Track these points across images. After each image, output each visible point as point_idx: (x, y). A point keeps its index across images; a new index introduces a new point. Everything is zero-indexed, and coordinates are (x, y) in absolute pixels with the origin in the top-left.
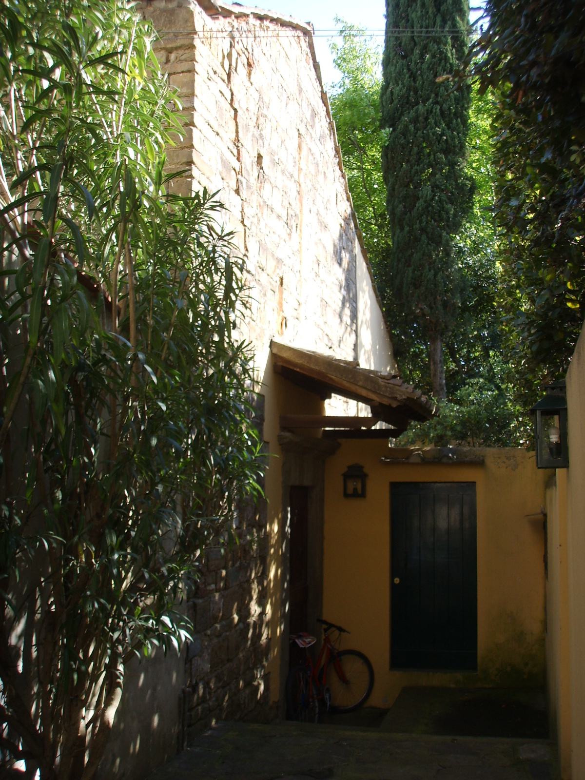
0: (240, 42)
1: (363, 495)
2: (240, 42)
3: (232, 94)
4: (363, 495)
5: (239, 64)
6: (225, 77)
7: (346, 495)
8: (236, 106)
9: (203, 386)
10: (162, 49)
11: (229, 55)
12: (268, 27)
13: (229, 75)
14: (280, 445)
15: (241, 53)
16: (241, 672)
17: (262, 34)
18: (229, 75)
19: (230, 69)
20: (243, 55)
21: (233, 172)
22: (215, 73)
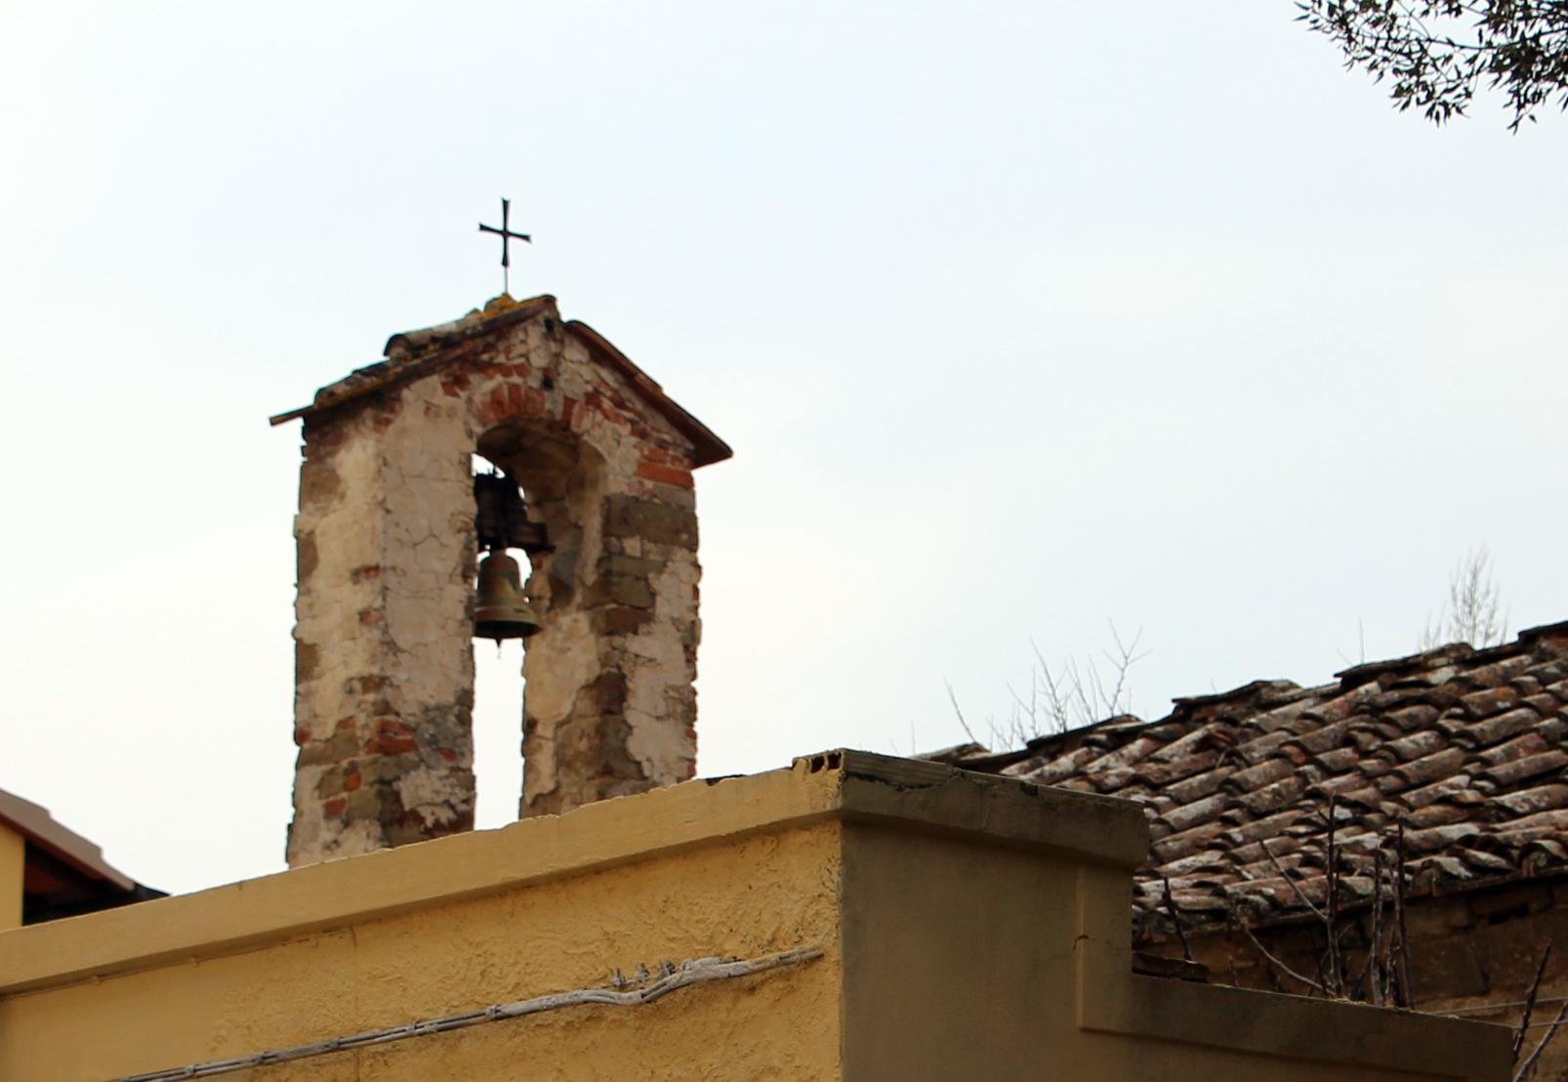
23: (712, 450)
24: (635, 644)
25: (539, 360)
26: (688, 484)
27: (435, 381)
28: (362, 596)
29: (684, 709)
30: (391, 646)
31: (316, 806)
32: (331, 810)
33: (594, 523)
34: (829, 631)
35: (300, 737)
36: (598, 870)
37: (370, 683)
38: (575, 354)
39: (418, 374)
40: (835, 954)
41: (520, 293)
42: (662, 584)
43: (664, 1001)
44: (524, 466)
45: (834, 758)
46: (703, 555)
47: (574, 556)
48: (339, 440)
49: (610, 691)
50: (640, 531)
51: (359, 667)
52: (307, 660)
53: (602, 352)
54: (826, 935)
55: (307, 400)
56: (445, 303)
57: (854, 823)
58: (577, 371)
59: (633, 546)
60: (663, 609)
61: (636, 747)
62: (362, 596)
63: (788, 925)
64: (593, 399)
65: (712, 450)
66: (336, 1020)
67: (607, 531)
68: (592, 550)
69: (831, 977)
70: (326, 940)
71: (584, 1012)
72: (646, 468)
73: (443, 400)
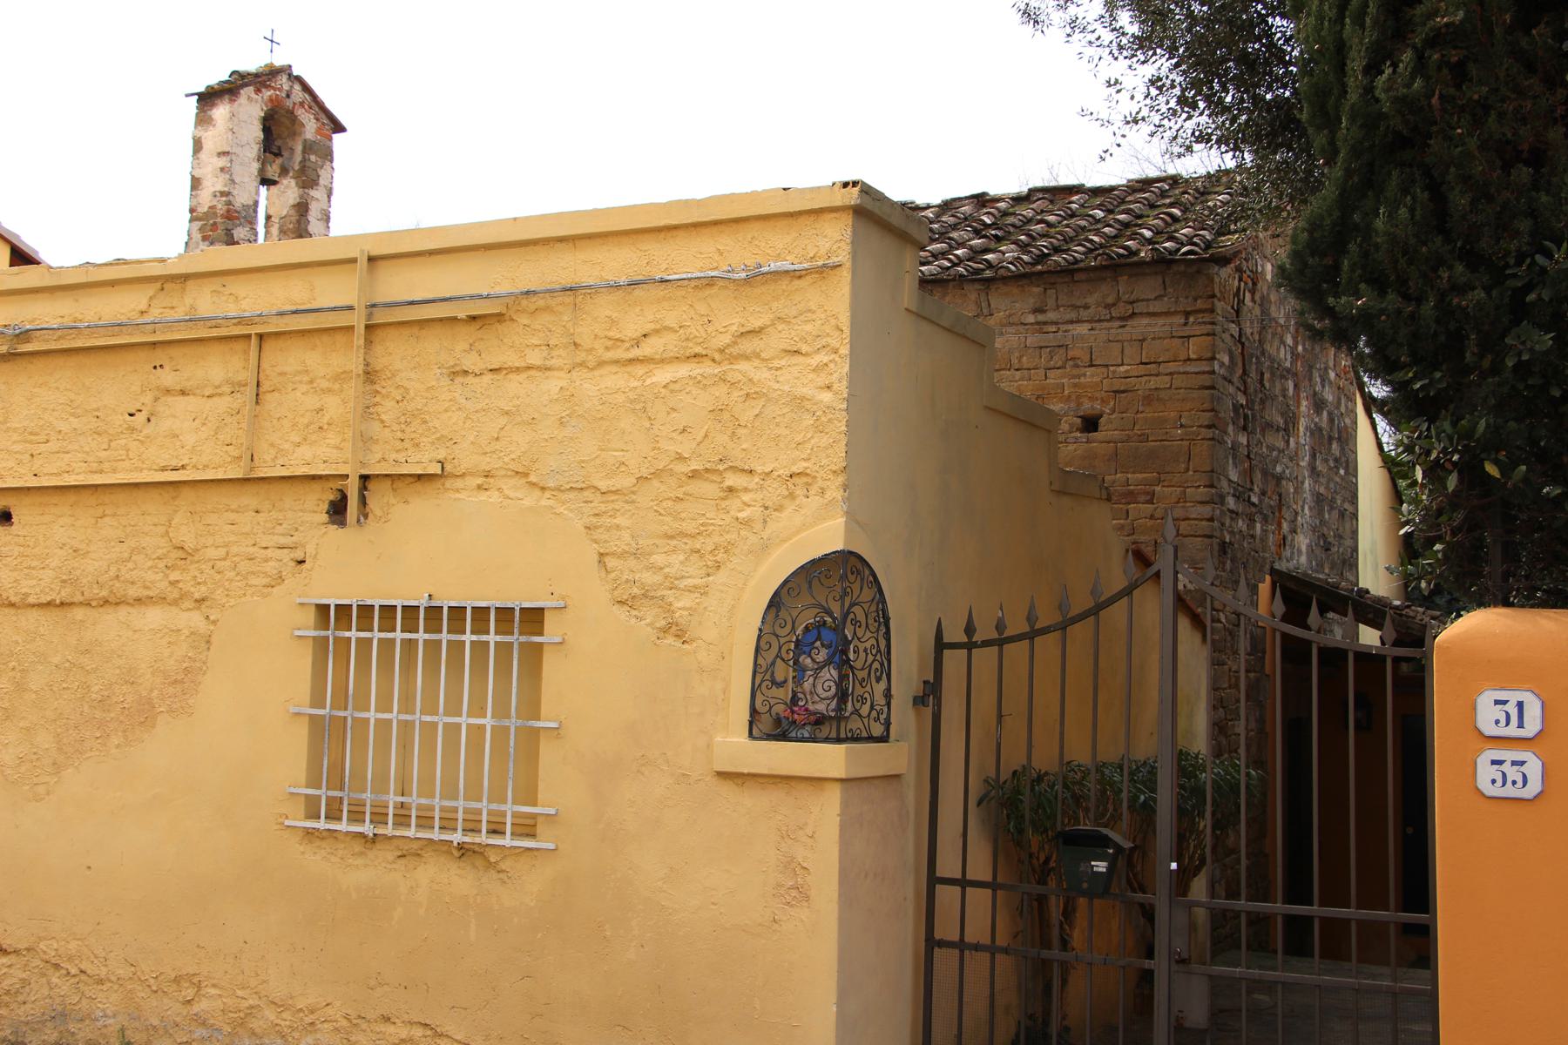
23: (339, 128)
24: (312, 193)
25: (286, 87)
26: (331, 139)
27: (252, 88)
28: (223, 162)
29: (326, 218)
30: (233, 181)
31: (197, 236)
32: (205, 239)
33: (299, 148)
34: (367, 195)
35: (192, 211)
36: (716, 223)
37: (223, 194)
38: (297, 87)
39: (246, 85)
40: (848, 265)
41: (278, 63)
42: (322, 172)
43: (757, 278)
44: (284, 126)
45: (855, 184)
46: (335, 164)
47: (290, 159)
48: (213, 105)
49: (302, 208)
50: (315, 153)
51: (220, 187)
52: (196, 183)
53: (306, 88)
54: (843, 255)
55: (202, 89)
56: (252, 63)
57: (859, 212)
58: (298, 94)
59: (313, 158)
60: (322, 181)
61: (311, 229)
62: (223, 162)
63: (823, 251)
64: (302, 104)
65: (339, 128)
66: (567, 279)
67: (304, 151)
68: (298, 157)
69: (846, 275)
70: (559, 245)
71: (705, 282)
72: (318, 131)
73: (253, 95)
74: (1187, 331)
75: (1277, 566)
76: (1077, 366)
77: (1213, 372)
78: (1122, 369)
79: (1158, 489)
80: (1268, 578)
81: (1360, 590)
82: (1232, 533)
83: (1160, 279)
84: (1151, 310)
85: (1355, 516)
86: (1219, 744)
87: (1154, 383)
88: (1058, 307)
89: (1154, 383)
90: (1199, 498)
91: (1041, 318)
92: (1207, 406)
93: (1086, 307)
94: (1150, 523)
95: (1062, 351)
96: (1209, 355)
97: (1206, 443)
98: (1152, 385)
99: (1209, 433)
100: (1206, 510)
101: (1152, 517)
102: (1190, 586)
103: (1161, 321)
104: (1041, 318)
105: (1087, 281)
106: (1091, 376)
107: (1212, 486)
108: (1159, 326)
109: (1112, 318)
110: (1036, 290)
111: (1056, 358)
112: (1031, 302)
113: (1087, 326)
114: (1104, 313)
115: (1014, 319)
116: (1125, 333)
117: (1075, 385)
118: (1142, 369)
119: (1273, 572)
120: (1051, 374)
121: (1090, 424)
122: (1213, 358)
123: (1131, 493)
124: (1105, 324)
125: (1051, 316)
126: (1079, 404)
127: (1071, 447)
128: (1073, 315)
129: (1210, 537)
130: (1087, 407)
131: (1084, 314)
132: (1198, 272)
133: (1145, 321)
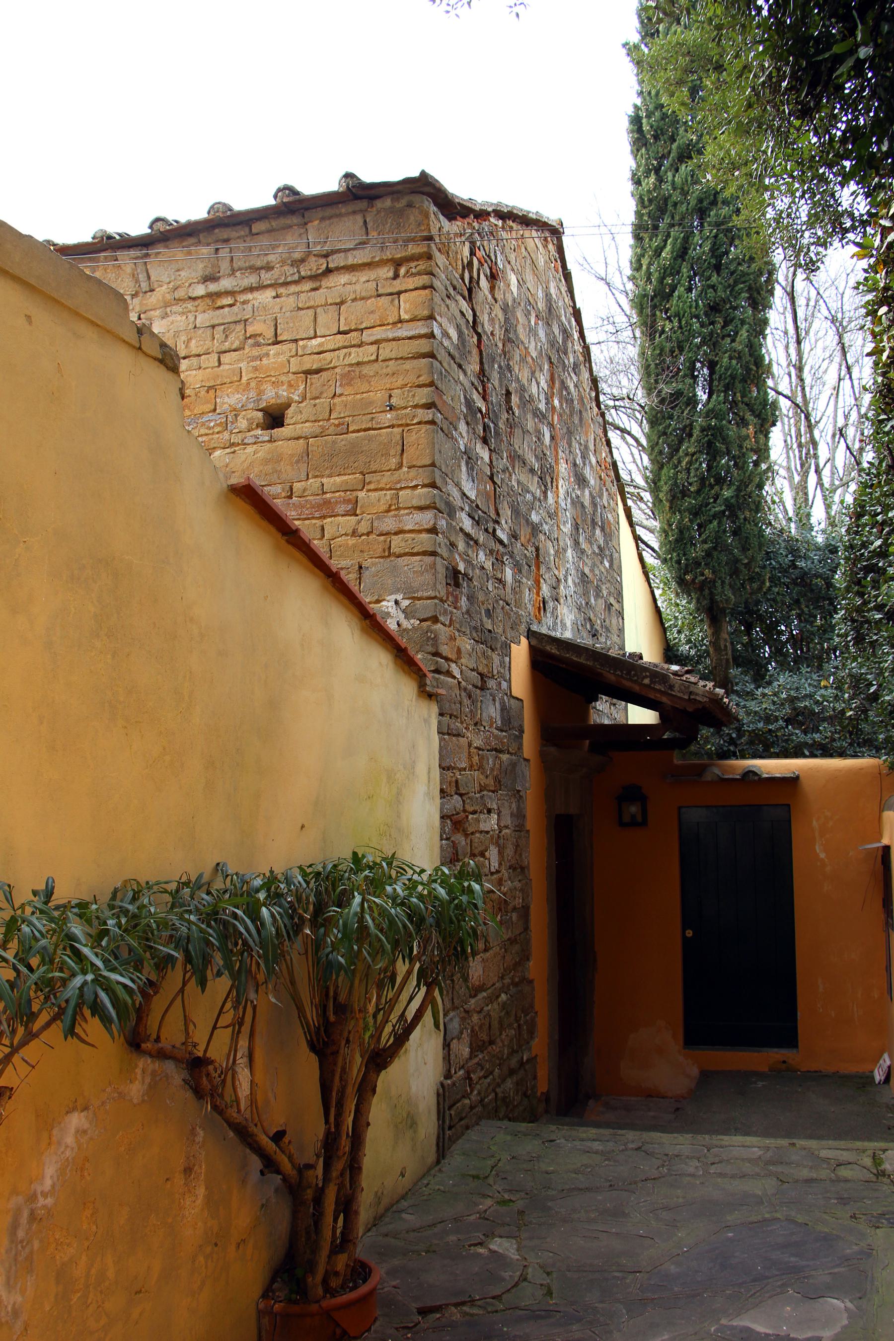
0: (481, 248)
1: (644, 823)
2: (481, 248)
3: (475, 315)
4: (644, 823)
5: (482, 276)
6: (466, 293)
7: (622, 824)
8: (480, 330)
9: (820, 32)
10: (388, 261)
11: (470, 264)
12: (511, 228)
13: (470, 291)
14: (543, 762)
15: (483, 261)
16: (505, 1057)
17: (504, 235)
18: (470, 291)
19: (470, 282)
20: (486, 265)
21: (479, 415)
22: (455, 289)
74: (398, 285)
75: (534, 628)
76: (258, 345)
77: (432, 336)
78: (314, 342)
79: (361, 494)
80: (524, 641)
81: (632, 655)
82: (469, 563)
83: (359, 219)
84: (350, 261)
85: (621, 614)
86: (454, 845)
87: (356, 355)
88: (233, 271)
89: (356, 355)
90: (415, 502)
91: (213, 287)
92: (424, 379)
93: (269, 268)
94: (351, 541)
95: (240, 327)
96: (426, 313)
97: (424, 428)
98: (353, 359)
99: (428, 415)
100: (426, 519)
101: (354, 533)
102: (406, 624)
103: (363, 276)
104: (213, 287)
105: (270, 231)
106: (276, 356)
107: (433, 485)
108: (362, 282)
109: (302, 279)
110: (205, 251)
111: (232, 337)
112: (200, 269)
113: (270, 293)
114: (290, 273)
115: (181, 293)
116: (319, 297)
117: (256, 369)
118: (340, 340)
119: (530, 634)
120: (226, 358)
121: (274, 418)
122: (431, 317)
123: (327, 502)
124: (293, 289)
125: (226, 284)
126: (260, 393)
127: (250, 449)
128: (252, 280)
129: (434, 554)
130: (271, 395)
131: (267, 277)
132: (410, 205)
133: (344, 278)
